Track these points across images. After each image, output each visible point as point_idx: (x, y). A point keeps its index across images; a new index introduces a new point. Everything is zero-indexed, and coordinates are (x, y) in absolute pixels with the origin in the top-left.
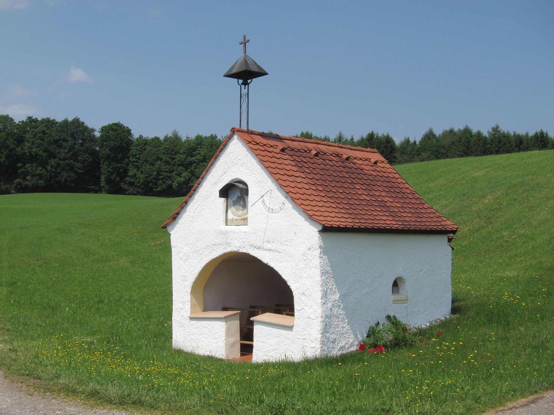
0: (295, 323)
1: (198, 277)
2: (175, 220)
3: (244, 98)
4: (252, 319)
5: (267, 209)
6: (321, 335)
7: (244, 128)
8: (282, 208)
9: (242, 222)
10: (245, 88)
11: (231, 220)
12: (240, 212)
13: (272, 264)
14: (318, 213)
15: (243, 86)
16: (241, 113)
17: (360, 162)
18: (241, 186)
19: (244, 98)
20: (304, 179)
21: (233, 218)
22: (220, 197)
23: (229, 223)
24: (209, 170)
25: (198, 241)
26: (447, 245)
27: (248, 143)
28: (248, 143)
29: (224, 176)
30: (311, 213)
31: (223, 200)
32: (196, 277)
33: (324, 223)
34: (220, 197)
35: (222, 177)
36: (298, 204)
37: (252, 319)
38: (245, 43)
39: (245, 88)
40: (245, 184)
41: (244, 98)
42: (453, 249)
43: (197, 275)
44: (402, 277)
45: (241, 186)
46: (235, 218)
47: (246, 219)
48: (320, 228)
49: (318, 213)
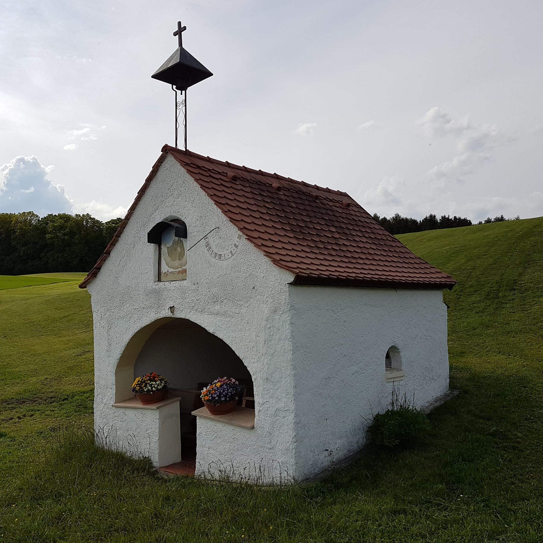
0: (255, 423)
1: (124, 351)
2: (95, 276)
3: (180, 107)
4: (193, 413)
5: (213, 255)
6: (295, 444)
7: (181, 147)
8: (233, 252)
9: (180, 276)
10: (181, 94)
11: (165, 273)
12: (177, 263)
13: (220, 335)
14: (288, 258)
15: (179, 92)
16: (176, 129)
17: (331, 204)
18: (175, 225)
19: (181, 108)
20: (262, 234)
21: (168, 271)
22: (149, 241)
23: (163, 278)
24: (135, 207)
25: (124, 303)
26: (442, 303)
27: (184, 165)
28: (184, 165)
29: (156, 214)
30: (277, 257)
31: (152, 247)
32: (122, 352)
33: (297, 271)
34: (149, 241)
35: (153, 216)
36: (258, 245)
37: (193, 413)
38: (180, 31)
39: (181, 94)
40: (184, 224)
41: (181, 108)
42: (448, 307)
43: (123, 349)
44: (396, 345)
45: (175, 225)
46: (171, 270)
47: (185, 271)
48: (291, 278)
49: (288, 258)
